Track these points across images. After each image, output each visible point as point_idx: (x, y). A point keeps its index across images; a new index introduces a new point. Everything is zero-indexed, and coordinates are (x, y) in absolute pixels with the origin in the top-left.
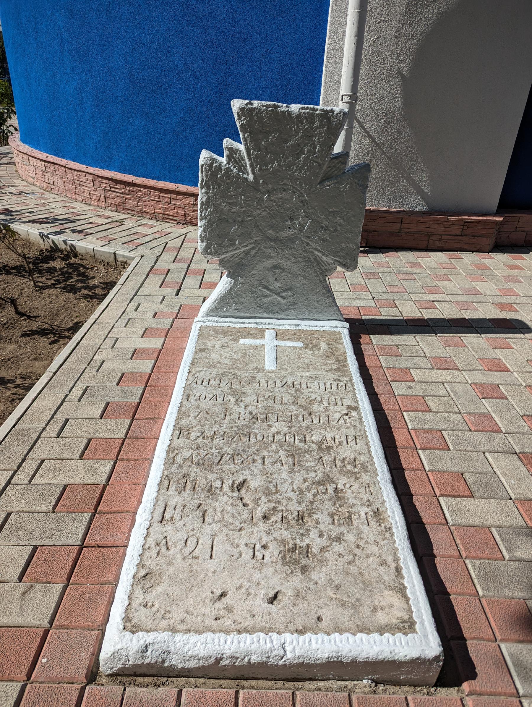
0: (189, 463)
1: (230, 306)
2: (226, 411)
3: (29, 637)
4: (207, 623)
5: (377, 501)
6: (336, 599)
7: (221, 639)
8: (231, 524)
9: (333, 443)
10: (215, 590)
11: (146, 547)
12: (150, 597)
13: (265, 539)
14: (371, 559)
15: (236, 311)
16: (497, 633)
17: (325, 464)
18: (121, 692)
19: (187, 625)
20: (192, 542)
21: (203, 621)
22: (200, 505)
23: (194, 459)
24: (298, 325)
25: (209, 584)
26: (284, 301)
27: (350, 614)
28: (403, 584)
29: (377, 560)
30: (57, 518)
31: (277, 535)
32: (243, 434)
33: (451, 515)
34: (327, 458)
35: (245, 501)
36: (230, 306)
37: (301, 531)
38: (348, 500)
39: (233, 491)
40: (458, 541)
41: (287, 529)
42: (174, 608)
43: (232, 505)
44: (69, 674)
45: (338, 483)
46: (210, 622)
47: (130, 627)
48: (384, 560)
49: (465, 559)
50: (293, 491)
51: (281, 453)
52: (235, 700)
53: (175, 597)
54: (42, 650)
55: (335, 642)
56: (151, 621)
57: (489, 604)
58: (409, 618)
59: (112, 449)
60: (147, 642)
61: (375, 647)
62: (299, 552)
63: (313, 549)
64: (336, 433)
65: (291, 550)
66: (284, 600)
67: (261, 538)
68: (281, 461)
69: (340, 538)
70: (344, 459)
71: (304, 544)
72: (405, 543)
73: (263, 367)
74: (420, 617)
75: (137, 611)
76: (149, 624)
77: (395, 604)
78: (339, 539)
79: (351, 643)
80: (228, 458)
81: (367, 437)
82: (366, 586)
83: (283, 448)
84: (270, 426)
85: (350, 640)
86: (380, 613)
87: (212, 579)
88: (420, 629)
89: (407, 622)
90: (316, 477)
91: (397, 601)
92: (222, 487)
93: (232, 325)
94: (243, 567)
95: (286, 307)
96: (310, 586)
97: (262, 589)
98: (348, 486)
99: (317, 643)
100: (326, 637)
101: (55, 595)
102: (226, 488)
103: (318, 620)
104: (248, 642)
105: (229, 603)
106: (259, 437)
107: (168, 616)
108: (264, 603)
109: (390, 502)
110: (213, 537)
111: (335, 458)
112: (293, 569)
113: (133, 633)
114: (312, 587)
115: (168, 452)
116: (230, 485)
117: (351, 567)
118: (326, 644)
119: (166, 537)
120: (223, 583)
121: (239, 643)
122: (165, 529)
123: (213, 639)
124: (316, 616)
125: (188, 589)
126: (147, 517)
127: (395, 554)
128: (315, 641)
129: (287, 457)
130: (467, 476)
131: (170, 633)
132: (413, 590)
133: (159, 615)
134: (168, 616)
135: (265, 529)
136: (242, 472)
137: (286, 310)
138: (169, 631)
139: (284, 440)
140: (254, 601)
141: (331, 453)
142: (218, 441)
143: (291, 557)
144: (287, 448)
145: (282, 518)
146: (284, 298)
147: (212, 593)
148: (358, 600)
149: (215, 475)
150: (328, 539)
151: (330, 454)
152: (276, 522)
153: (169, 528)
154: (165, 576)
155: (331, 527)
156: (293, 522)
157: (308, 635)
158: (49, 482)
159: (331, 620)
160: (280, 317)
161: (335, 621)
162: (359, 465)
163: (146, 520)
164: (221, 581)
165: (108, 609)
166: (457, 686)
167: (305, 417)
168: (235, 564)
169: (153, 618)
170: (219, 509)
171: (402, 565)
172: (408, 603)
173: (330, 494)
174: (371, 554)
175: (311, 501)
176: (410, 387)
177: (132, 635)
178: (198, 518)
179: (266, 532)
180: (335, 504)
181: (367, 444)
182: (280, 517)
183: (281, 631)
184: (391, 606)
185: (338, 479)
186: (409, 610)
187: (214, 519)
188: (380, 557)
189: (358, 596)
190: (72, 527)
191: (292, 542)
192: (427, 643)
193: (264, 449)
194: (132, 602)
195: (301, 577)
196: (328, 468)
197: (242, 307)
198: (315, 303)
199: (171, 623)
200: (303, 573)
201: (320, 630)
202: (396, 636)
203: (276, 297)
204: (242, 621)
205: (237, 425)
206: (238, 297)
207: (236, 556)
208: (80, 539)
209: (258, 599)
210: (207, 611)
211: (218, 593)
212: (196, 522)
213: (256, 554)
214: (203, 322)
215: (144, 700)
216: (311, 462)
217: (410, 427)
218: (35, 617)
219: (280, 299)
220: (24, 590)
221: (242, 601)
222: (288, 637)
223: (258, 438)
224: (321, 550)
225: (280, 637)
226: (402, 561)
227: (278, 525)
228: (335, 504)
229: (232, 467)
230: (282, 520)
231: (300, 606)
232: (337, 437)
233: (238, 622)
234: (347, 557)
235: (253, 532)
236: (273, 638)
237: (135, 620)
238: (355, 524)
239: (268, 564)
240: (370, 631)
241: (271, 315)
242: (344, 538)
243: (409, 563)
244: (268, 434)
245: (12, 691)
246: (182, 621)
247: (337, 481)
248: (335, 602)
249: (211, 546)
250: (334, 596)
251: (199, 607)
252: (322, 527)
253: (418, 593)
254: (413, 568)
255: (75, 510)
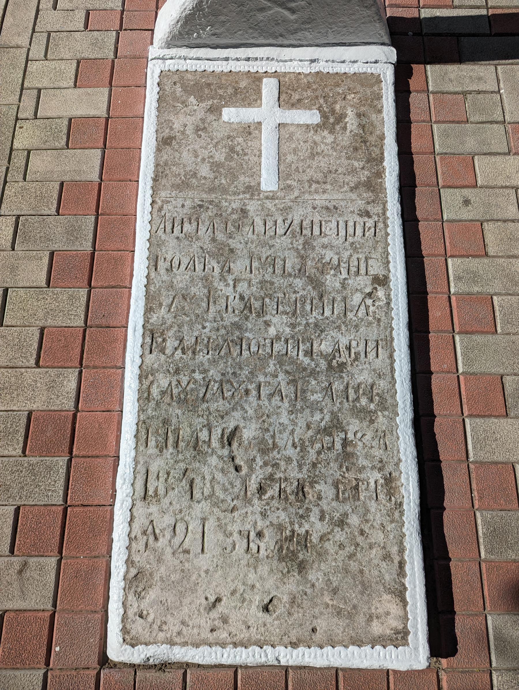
0: (167, 399)
1: (204, 30)
2: (209, 292)
3: (37, 624)
4: (203, 636)
5: (391, 460)
6: (332, 606)
7: (218, 653)
8: (222, 501)
9: (347, 356)
10: (209, 596)
11: (133, 536)
12: (145, 604)
13: (260, 525)
14: (374, 551)
15: (214, 38)
16: (488, 603)
17: (334, 395)
18: (133, 677)
19: (184, 638)
20: (180, 528)
21: (199, 633)
22: (186, 470)
23: (174, 392)
24: (313, 61)
25: (202, 589)
26: (293, 17)
27: (344, 625)
28: (404, 585)
29: (381, 552)
30: (31, 468)
31: (273, 517)
32: (232, 341)
33: (474, 448)
34: (338, 386)
35: (238, 461)
36: (204, 30)
37: (301, 512)
38: (357, 460)
39: (223, 447)
40: (474, 486)
41: (285, 509)
42: (170, 619)
43: (222, 470)
44: (83, 663)
45: (349, 430)
46: (206, 634)
47: (129, 640)
48: (389, 552)
49: (477, 510)
50: (294, 446)
51: (281, 376)
52: (234, 681)
53: (169, 604)
54: (53, 634)
55: (327, 656)
56: (149, 633)
57: (488, 570)
58: (404, 628)
59: (72, 349)
60: (148, 656)
61: (365, 661)
62: (297, 541)
63: (312, 538)
64: (352, 337)
65: (289, 538)
66: (281, 610)
67: (256, 523)
68: (281, 391)
69: (342, 521)
70: (359, 385)
71: (302, 531)
72: (415, 526)
73: (259, 184)
74: (415, 626)
75: (134, 622)
76: (146, 636)
77: (392, 611)
78: (342, 523)
79: (342, 657)
80: (215, 388)
81: (392, 339)
82: (365, 587)
83: (284, 368)
84: (267, 324)
85: (341, 654)
86: (375, 623)
87: (206, 581)
88: (412, 641)
89: (400, 633)
90: (322, 420)
91: (394, 609)
92: (210, 439)
93: (210, 67)
94: (237, 564)
95: (296, 26)
96: (306, 590)
97: (257, 594)
98: (359, 435)
99: (310, 657)
100: (318, 650)
101: (51, 574)
102: (215, 444)
103: (313, 630)
104: (244, 656)
105: (223, 612)
106: (254, 349)
107: (165, 627)
108: (259, 612)
109: (406, 461)
110: (204, 520)
111: (348, 384)
112: (290, 566)
113: (133, 646)
114: (309, 591)
115: (140, 377)
116: (219, 436)
117: (351, 562)
118: (319, 659)
119: (152, 521)
120: (217, 586)
121: (235, 657)
122: (150, 510)
123: (211, 654)
124: (311, 628)
125: (182, 595)
126: (128, 491)
127: (401, 543)
128: (308, 656)
129: (288, 384)
130: (508, 380)
131: (169, 646)
132: (413, 592)
133: (155, 627)
134: (165, 627)
135: (260, 509)
136: (233, 414)
137: (295, 32)
138: (167, 644)
139: (284, 351)
140: (249, 609)
141: (344, 375)
142: (202, 358)
143: (288, 548)
144: (288, 368)
145: (280, 491)
146: (293, 11)
147: (206, 599)
148: (355, 607)
149: (201, 420)
150: (329, 523)
151: (341, 377)
152: (273, 498)
153: (154, 509)
154: (157, 577)
155: (334, 504)
156: (292, 498)
157: (301, 649)
158: (9, 409)
159: (325, 632)
160: (286, 42)
161: (329, 632)
162: (377, 398)
163: (127, 496)
164: (214, 583)
165: (107, 586)
166: (436, 657)
167: (314, 302)
168: (228, 561)
169: (150, 630)
170: (208, 477)
171: (406, 558)
172: (405, 609)
173: (337, 450)
174: (375, 543)
175: (314, 463)
176: (467, 202)
177: (132, 649)
178: (185, 493)
179: (261, 513)
180: (341, 467)
181: (391, 356)
182: (277, 490)
183: (276, 643)
184: (388, 613)
185: (348, 424)
186: (406, 619)
187: (203, 493)
188: (384, 548)
189: (355, 601)
190: (50, 481)
191: (289, 528)
192: (417, 656)
193: (260, 370)
194: (127, 610)
195: (298, 577)
196: (338, 405)
197: (222, 29)
198: (345, 18)
199: (168, 636)
200: (300, 572)
201: (314, 642)
202: (387, 648)
203: (280, 10)
204: (238, 633)
205: (225, 323)
206: (215, 14)
207: (229, 549)
208: (61, 499)
209: (253, 607)
210: (203, 622)
211: (212, 599)
212: (183, 499)
213: (251, 544)
214: (163, 59)
215: (154, 683)
216: (316, 392)
217: (452, 290)
218: (38, 601)
219: (286, 13)
220: (18, 568)
221: (237, 610)
222: (281, 649)
223: (252, 350)
224: (321, 538)
225: (275, 651)
226: (407, 552)
227: (275, 503)
228: (341, 467)
229: (220, 405)
230: (280, 495)
231: (296, 615)
232: (354, 344)
233: (234, 634)
234: (348, 549)
235: (247, 513)
236: (267, 651)
237: (133, 633)
238: (362, 498)
239: (263, 559)
240: (363, 643)
241: (271, 41)
242: (347, 521)
243: (415, 556)
244: (265, 339)
245: (36, 681)
246: (179, 633)
247: (347, 428)
248: (331, 610)
249: (201, 535)
250: (330, 603)
251: (194, 617)
252: (324, 504)
253: (418, 597)
254: (418, 563)
255: (48, 454)
